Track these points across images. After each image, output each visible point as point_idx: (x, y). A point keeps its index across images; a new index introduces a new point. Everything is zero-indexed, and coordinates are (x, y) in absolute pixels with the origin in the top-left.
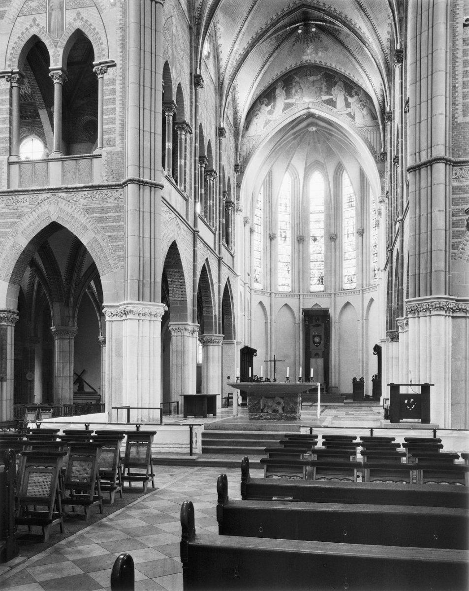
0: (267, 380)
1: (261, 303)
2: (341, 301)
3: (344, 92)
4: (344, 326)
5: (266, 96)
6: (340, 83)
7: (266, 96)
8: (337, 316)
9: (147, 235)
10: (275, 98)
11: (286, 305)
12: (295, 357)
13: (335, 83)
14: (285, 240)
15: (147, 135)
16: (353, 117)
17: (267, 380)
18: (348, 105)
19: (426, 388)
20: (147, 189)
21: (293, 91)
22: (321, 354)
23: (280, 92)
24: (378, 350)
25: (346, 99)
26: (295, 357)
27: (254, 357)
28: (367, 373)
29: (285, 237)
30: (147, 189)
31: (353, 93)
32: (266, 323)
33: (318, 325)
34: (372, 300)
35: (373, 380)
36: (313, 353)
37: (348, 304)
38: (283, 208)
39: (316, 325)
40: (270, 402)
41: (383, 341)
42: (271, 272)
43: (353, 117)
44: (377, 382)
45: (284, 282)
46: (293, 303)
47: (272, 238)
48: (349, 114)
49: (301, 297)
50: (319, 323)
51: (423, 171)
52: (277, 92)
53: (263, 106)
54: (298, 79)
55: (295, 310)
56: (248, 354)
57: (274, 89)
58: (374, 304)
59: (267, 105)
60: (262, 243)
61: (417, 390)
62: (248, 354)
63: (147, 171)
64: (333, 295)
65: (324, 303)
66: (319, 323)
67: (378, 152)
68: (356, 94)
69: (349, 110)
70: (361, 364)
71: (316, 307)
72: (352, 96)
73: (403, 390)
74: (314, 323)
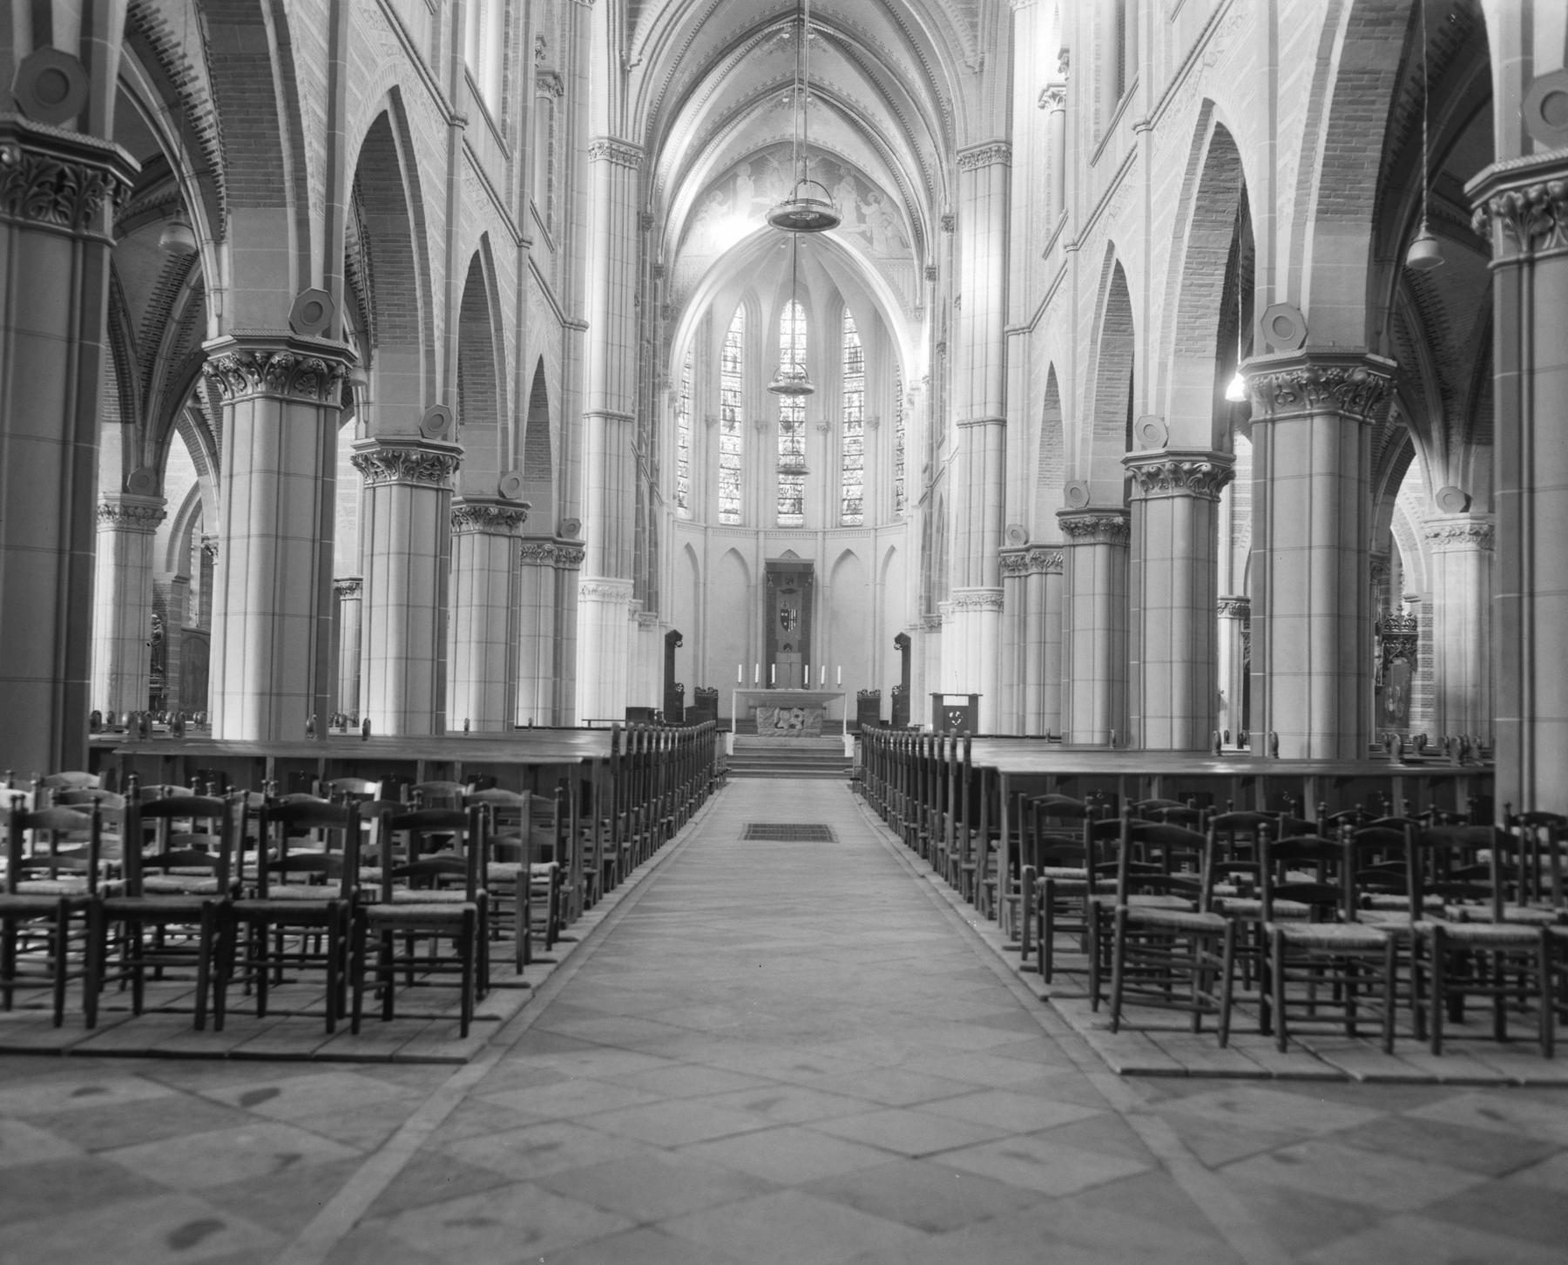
0: (112, 725)
1: (688, 547)
2: (836, 546)
3: (854, 195)
4: (840, 589)
5: (721, 183)
6: (849, 179)
7: (721, 183)
8: (827, 579)
9: (614, 486)
10: (735, 189)
11: (733, 551)
12: (748, 651)
13: (841, 178)
14: (732, 428)
15: (616, 348)
16: (870, 240)
17: (112, 725)
18: (861, 218)
19: (974, 699)
20: (615, 422)
21: (768, 184)
22: (795, 645)
23: (744, 170)
24: (903, 642)
25: (858, 208)
26: (748, 651)
27: (677, 650)
28: (882, 683)
29: (733, 420)
30: (615, 422)
31: (870, 198)
32: (696, 584)
33: (791, 591)
34: (892, 549)
35: (893, 695)
36: (781, 645)
37: (848, 553)
38: (730, 365)
39: (789, 587)
40: (785, 714)
41: (914, 628)
42: (707, 487)
43: (870, 240)
44: (901, 700)
45: (729, 506)
46: (746, 546)
47: (710, 422)
48: (863, 234)
49: (761, 535)
50: (794, 586)
51: (976, 429)
52: (740, 181)
53: (714, 205)
54: (776, 164)
55: (750, 560)
56: (673, 639)
57: (736, 176)
58: (895, 557)
59: (721, 204)
60: (691, 433)
61: (964, 702)
62: (673, 639)
63: (615, 399)
64: (820, 535)
65: (805, 551)
66: (794, 586)
67: (911, 305)
68: (876, 201)
69: (863, 227)
70: (870, 664)
71: (786, 559)
72: (868, 204)
73: (947, 701)
74: (785, 587)
